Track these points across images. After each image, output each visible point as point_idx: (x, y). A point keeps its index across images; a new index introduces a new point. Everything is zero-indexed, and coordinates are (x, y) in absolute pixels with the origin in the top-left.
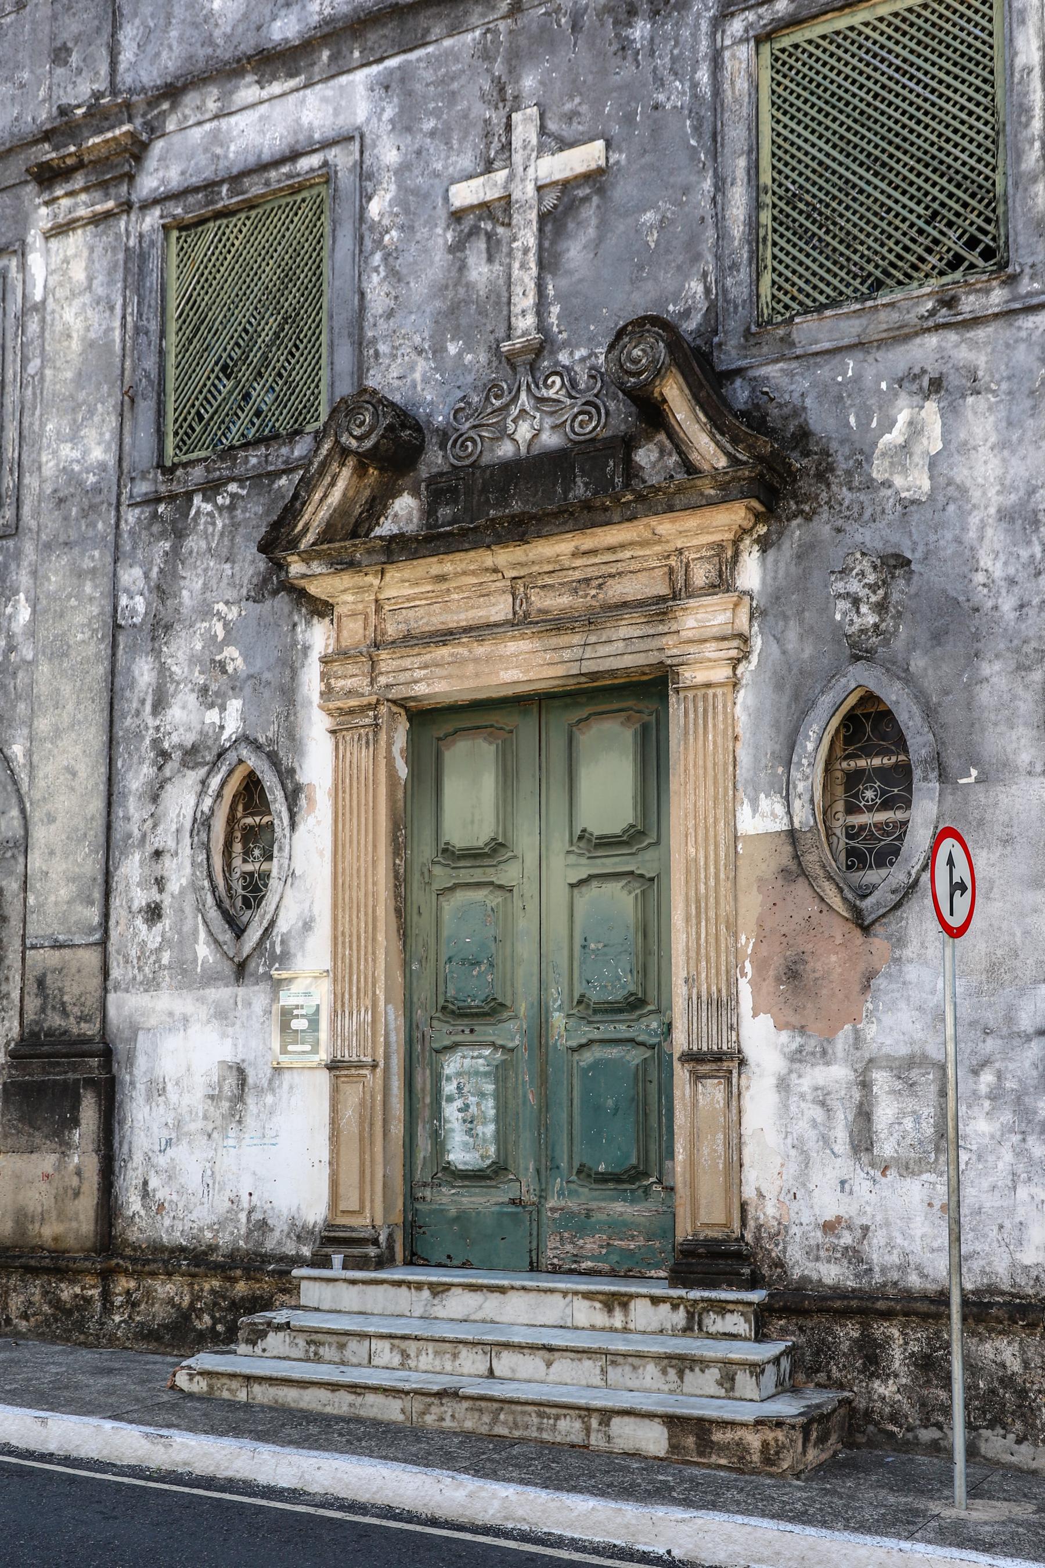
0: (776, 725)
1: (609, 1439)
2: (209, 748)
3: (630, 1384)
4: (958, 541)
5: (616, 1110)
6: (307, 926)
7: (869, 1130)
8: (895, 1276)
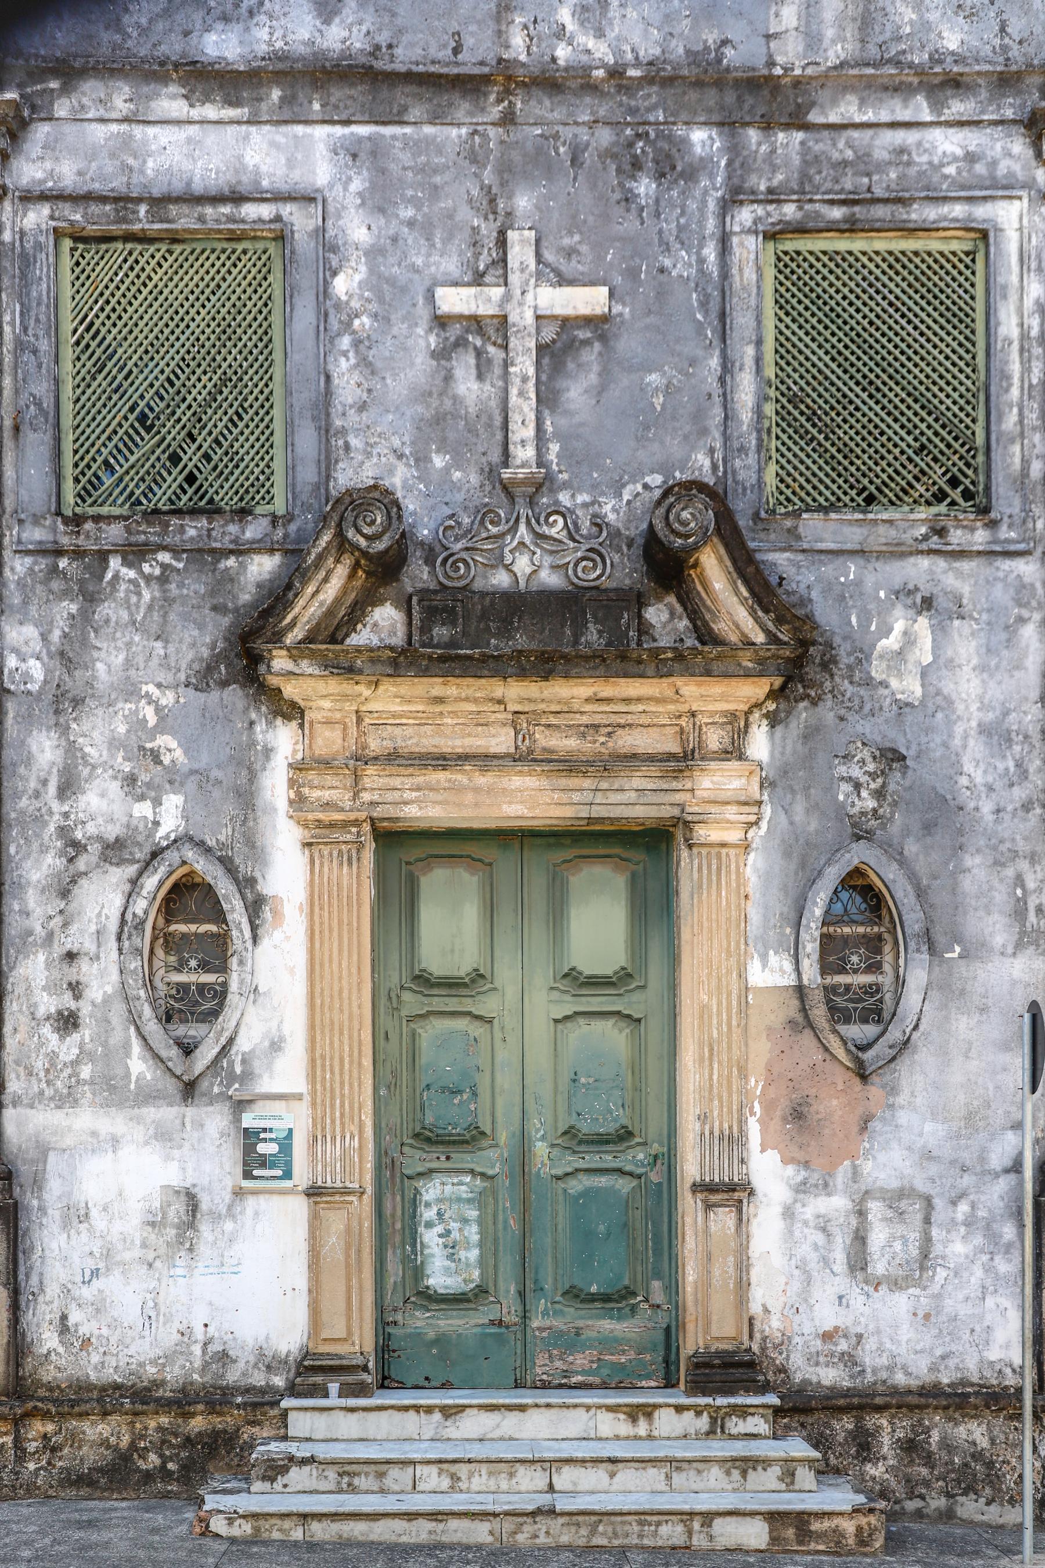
0: (784, 889)
1: (711, 1538)
2: (139, 845)
3: (695, 1487)
4: (945, 745)
5: (609, 1234)
6: (276, 1046)
7: (864, 1252)
8: (884, 1375)
